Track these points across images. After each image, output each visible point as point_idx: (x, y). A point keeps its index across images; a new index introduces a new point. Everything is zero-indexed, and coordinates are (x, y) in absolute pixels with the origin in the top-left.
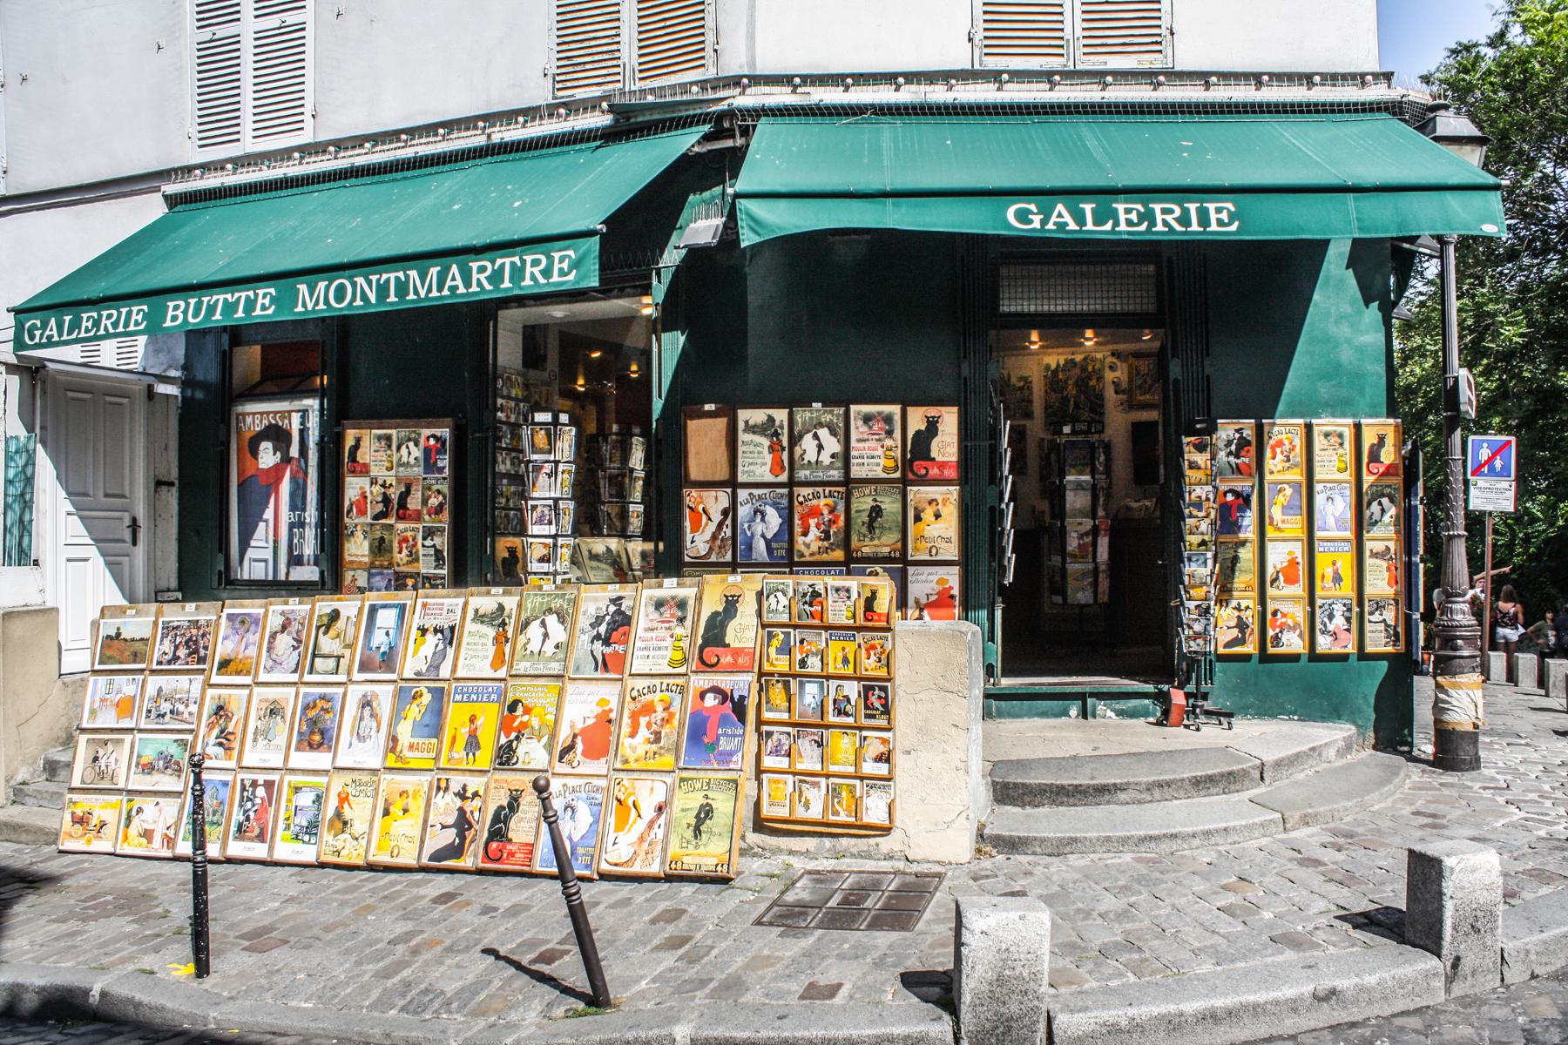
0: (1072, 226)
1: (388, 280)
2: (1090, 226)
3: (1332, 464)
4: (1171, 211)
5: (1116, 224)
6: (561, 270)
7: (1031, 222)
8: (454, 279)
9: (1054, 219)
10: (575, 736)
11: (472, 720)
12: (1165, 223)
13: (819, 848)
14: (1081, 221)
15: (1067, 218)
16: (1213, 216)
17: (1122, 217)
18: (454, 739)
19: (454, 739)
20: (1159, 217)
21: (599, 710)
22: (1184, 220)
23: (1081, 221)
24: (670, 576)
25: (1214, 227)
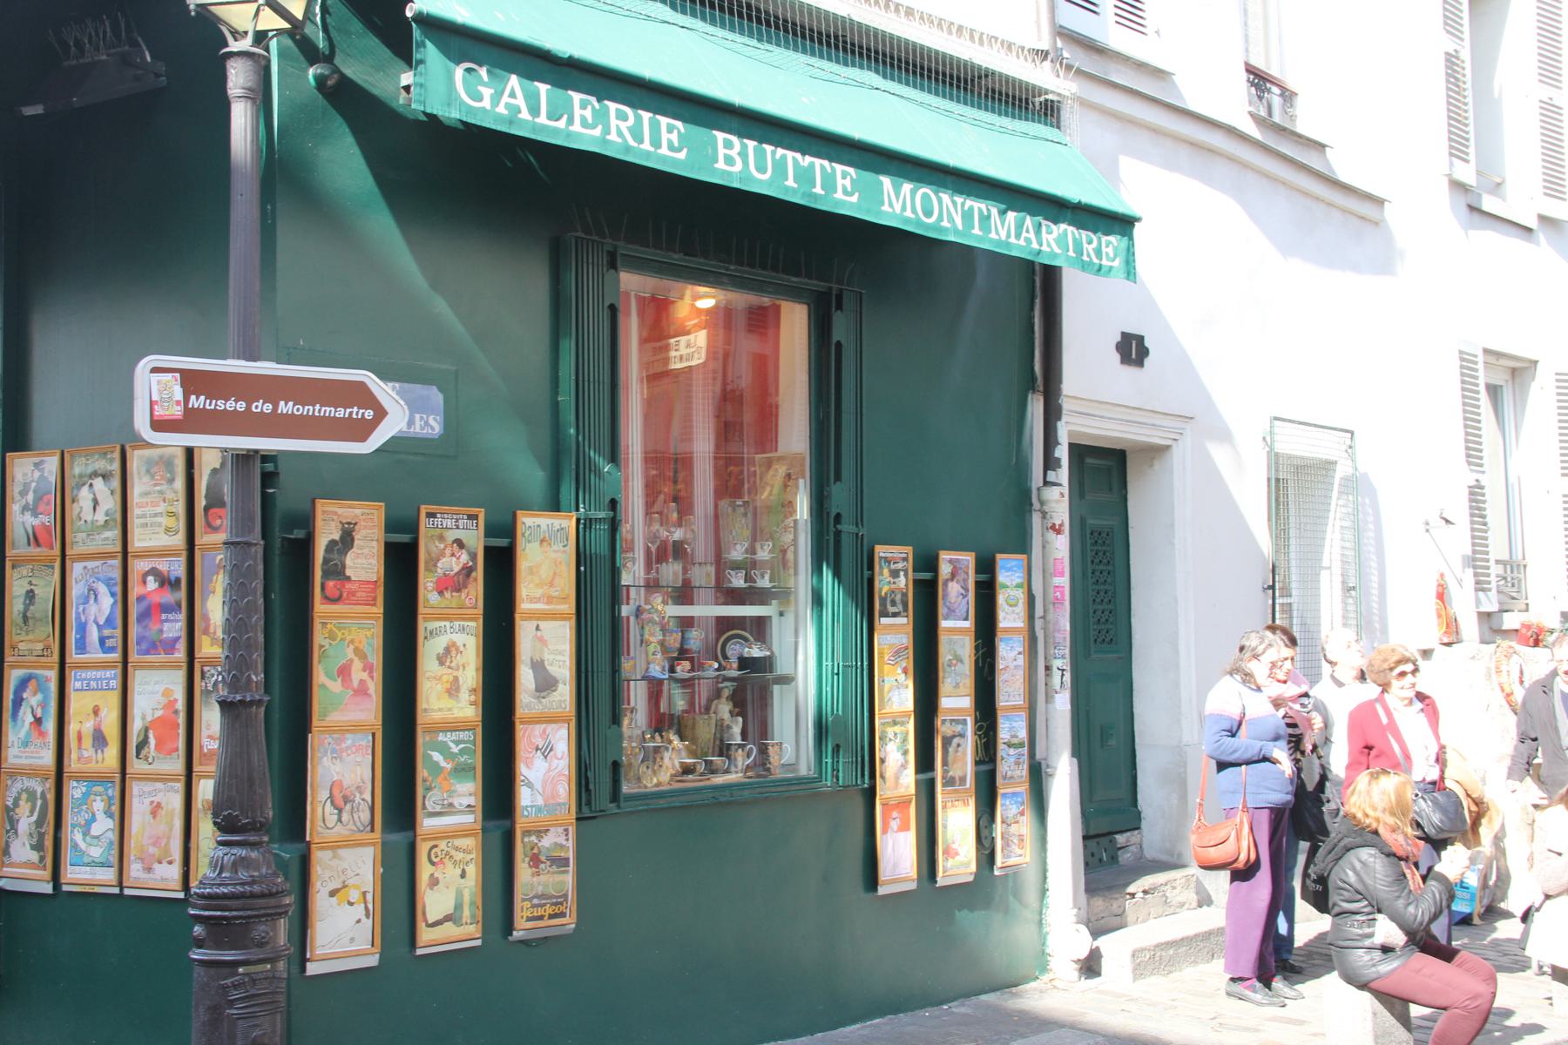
0: (525, 115)
1: (971, 209)
2: (543, 119)
3: (789, 748)
4: (625, 119)
5: (571, 121)
6: (670, 142)
7: (481, 100)
8: (513, 95)
9: (505, 99)
10: (147, 730)
11: (96, 711)
12: (620, 134)
13: (249, 646)
14: (535, 111)
15: (520, 101)
16: (665, 136)
17: (577, 112)
18: (80, 738)
19: (80, 738)
20: (614, 122)
21: (164, 701)
22: (637, 134)
23: (535, 111)
24: (217, 792)
25: (664, 151)
